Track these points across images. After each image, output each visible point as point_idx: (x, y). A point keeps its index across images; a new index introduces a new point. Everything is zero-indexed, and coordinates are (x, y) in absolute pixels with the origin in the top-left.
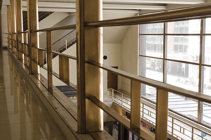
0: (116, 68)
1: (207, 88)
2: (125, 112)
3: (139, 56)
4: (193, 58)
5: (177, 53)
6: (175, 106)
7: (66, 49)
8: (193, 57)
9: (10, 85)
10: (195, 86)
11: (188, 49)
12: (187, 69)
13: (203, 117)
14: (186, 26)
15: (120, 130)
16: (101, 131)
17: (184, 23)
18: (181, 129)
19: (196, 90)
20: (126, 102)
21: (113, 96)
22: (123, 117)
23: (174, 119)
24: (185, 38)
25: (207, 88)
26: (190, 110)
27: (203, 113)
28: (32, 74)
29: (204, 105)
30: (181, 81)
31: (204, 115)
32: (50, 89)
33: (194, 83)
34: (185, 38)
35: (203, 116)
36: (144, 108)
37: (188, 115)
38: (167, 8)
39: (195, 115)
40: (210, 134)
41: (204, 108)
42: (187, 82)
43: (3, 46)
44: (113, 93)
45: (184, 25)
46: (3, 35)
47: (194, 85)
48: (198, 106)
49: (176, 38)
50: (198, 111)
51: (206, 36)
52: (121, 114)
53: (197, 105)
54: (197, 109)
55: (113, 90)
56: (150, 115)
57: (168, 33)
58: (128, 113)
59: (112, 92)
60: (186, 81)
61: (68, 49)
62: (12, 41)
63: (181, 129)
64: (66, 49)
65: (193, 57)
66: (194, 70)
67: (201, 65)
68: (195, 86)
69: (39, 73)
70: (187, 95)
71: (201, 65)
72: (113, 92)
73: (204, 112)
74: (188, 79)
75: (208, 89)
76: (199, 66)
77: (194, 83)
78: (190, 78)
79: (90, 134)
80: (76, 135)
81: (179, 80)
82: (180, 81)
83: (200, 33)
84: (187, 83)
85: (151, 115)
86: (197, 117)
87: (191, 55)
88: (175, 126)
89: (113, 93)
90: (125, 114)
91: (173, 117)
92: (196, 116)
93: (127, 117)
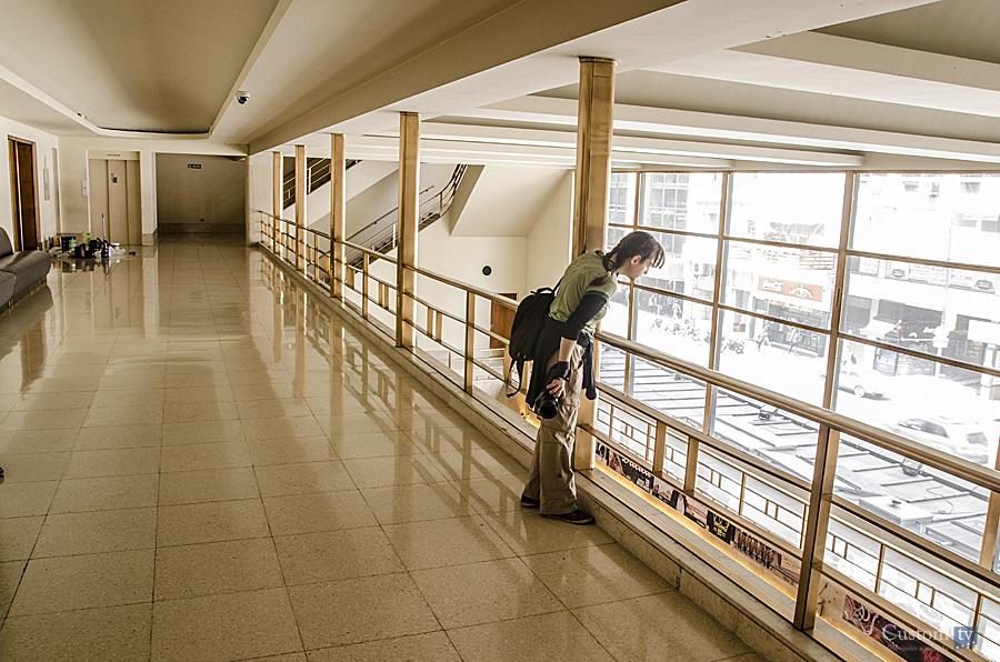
6: (654, 396)
9: (328, 417)
12: (753, 325)
13: (717, 423)
15: (705, 584)
18: (767, 504)
23: (984, 600)
29: (719, 395)
37: (682, 418)
38: (864, 162)
39: (698, 417)
40: (998, 599)
41: (720, 402)
46: (251, 216)
53: (703, 394)
54: (702, 403)
56: (629, 428)
57: (856, 247)
63: (767, 504)
66: (698, 316)
67: (717, 305)
70: (682, 369)
88: (748, 496)
92: (701, 420)
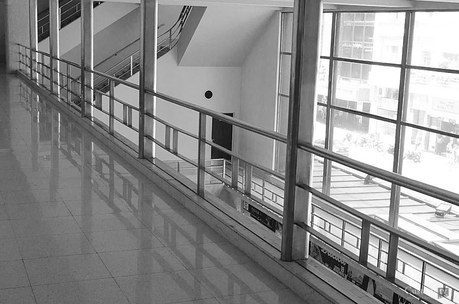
0: (231, 115)
1: (407, 157)
2: (248, 205)
3: (279, 95)
4: (381, 93)
5: (346, 79)
7: (131, 74)
8: (381, 90)
10: (382, 151)
11: (370, 72)
14: (367, 24)
16: (307, 259)
17: (365, 18)
19: (391, 170)
20: (273, 199)
21: (224, 173)
22: (244, 214)
24: (366, 51)
25: (407, 157)
26: (374, 206)
27: (399, 212)
28: (144, 158)
30: (353, 139)
31: (401, 217)
32: (200, 193)
33: (379, 145)
34: (365, 49)
35: (399, 218)
36: (346, 230)
42: (365, 142)
43: (11, 69)
44: (224, 168)
45: (364, 22)
47: (379, 149)
48: (390, 198)
49: (347, 49)
50: (390, 207)
51: (412, 70)
52: (239, 209)
54: (388, 203)
55: (225, 161)
58: (254, 207)
59: (223, 165)
60: (363, 139)
61: (134, 75)
62: (52, 72)
64: (131, 74)
65: (381, 90)
66: (385, 134)
67: (400, 123)
68: (382, 151)
69: (154, 157)
71: (400, 123)
72: (225, 166)
73: (401, 210)
74: (367, 136)
75: (408, 158)
76: (395, 125)
77: (379, 145)
78: (371, 135)
79: (296, 262)
80: (281, 262)
81: (349, 138)
82: (351, 141)
83: (400, 63)
84: (364, 144)
85: (276, 201)
86: (388, 220)
87: (375, 86)
89: (224, 168)
90: (247, 209)
91: (344, 221)
93: (251, 216)
